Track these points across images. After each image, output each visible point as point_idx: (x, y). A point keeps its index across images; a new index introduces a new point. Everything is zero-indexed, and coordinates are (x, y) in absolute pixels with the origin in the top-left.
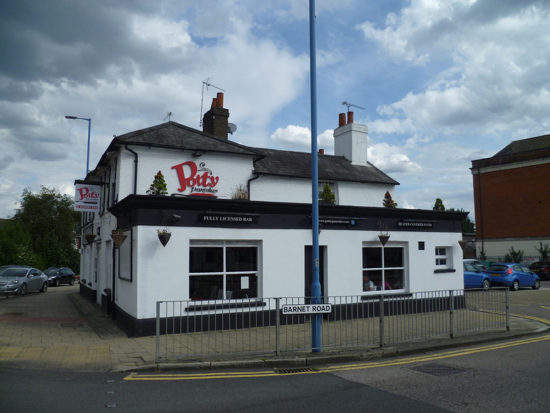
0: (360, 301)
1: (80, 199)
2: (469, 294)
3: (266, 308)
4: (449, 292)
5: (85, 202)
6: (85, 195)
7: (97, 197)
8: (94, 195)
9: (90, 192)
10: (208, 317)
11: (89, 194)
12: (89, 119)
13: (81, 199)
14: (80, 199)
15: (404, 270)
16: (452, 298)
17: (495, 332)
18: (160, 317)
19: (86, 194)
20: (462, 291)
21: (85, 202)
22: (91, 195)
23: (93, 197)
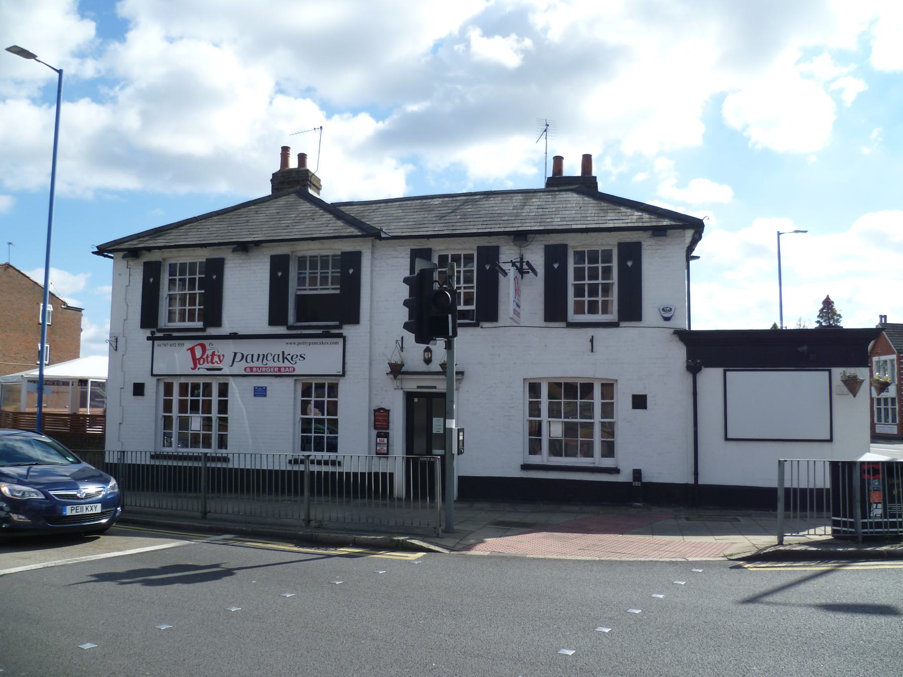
0: (149, 462)
1: (192, 368)
2: (826, 484)
3: (230, 466)
4: (140, 453)
5: (208, 369)
6: (199, 359)
7: (221, 361)
8: (215, 356)
9: (209, 352)
10: (823, 492)
11: (207, 355)
12: (58, 70)
13: (193, 367)
14: (192, 368)
15: (328, 384)
16: (119, 465)
17: (275, 544)
18: (785, 487)
19: (201, 357)
20: (362, 459)
21: (208, 369)
22: (210, 359)
23: (214, 362)
